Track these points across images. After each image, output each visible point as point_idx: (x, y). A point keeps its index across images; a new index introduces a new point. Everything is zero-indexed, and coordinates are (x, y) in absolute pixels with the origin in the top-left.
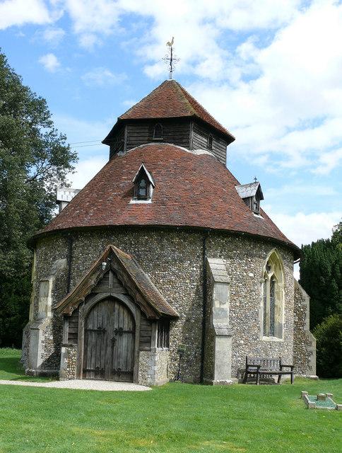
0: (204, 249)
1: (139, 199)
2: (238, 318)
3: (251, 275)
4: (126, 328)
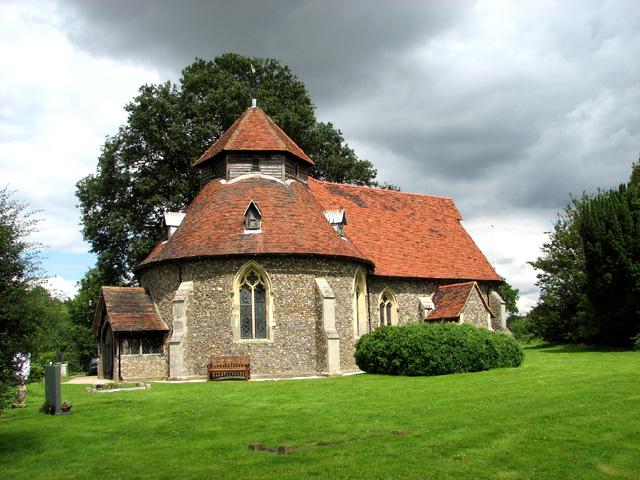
3: (220, 289)
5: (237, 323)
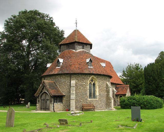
0: (70, 78)
1: (58, 67)
2: (80, 95)
3: (84, 83)
4: (48, 99)
5: (88, 94)
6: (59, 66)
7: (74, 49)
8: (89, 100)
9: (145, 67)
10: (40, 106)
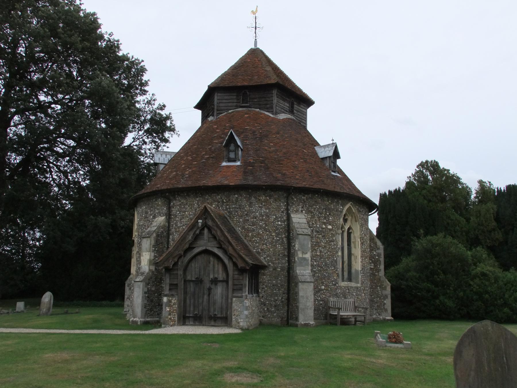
0: (288, 205)
3: (330, 227)
6: (234, 161)
7: (270, 109)
8: (341, 287)
9: (399, 188)
10: (179, 307)
